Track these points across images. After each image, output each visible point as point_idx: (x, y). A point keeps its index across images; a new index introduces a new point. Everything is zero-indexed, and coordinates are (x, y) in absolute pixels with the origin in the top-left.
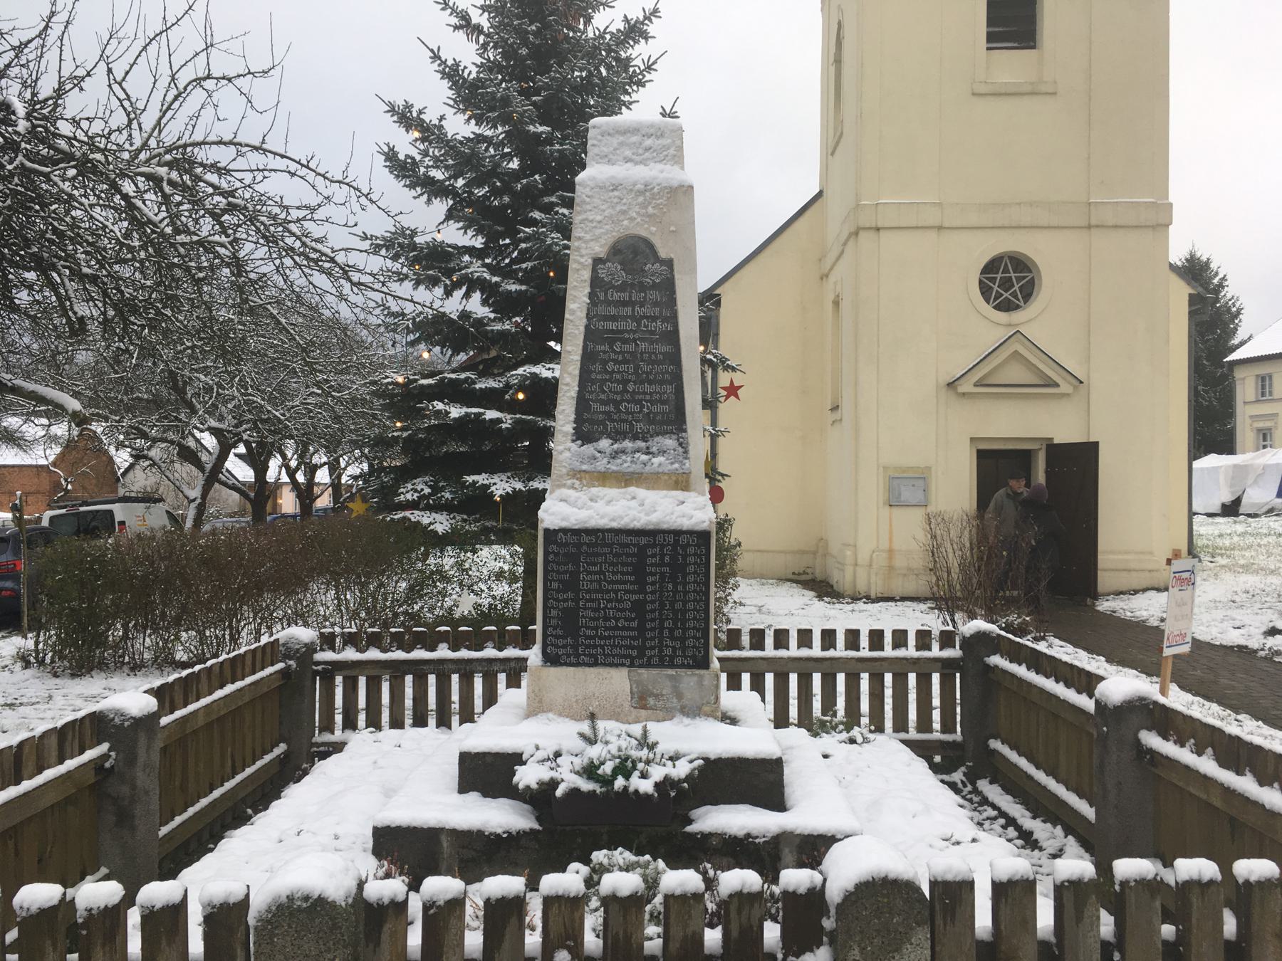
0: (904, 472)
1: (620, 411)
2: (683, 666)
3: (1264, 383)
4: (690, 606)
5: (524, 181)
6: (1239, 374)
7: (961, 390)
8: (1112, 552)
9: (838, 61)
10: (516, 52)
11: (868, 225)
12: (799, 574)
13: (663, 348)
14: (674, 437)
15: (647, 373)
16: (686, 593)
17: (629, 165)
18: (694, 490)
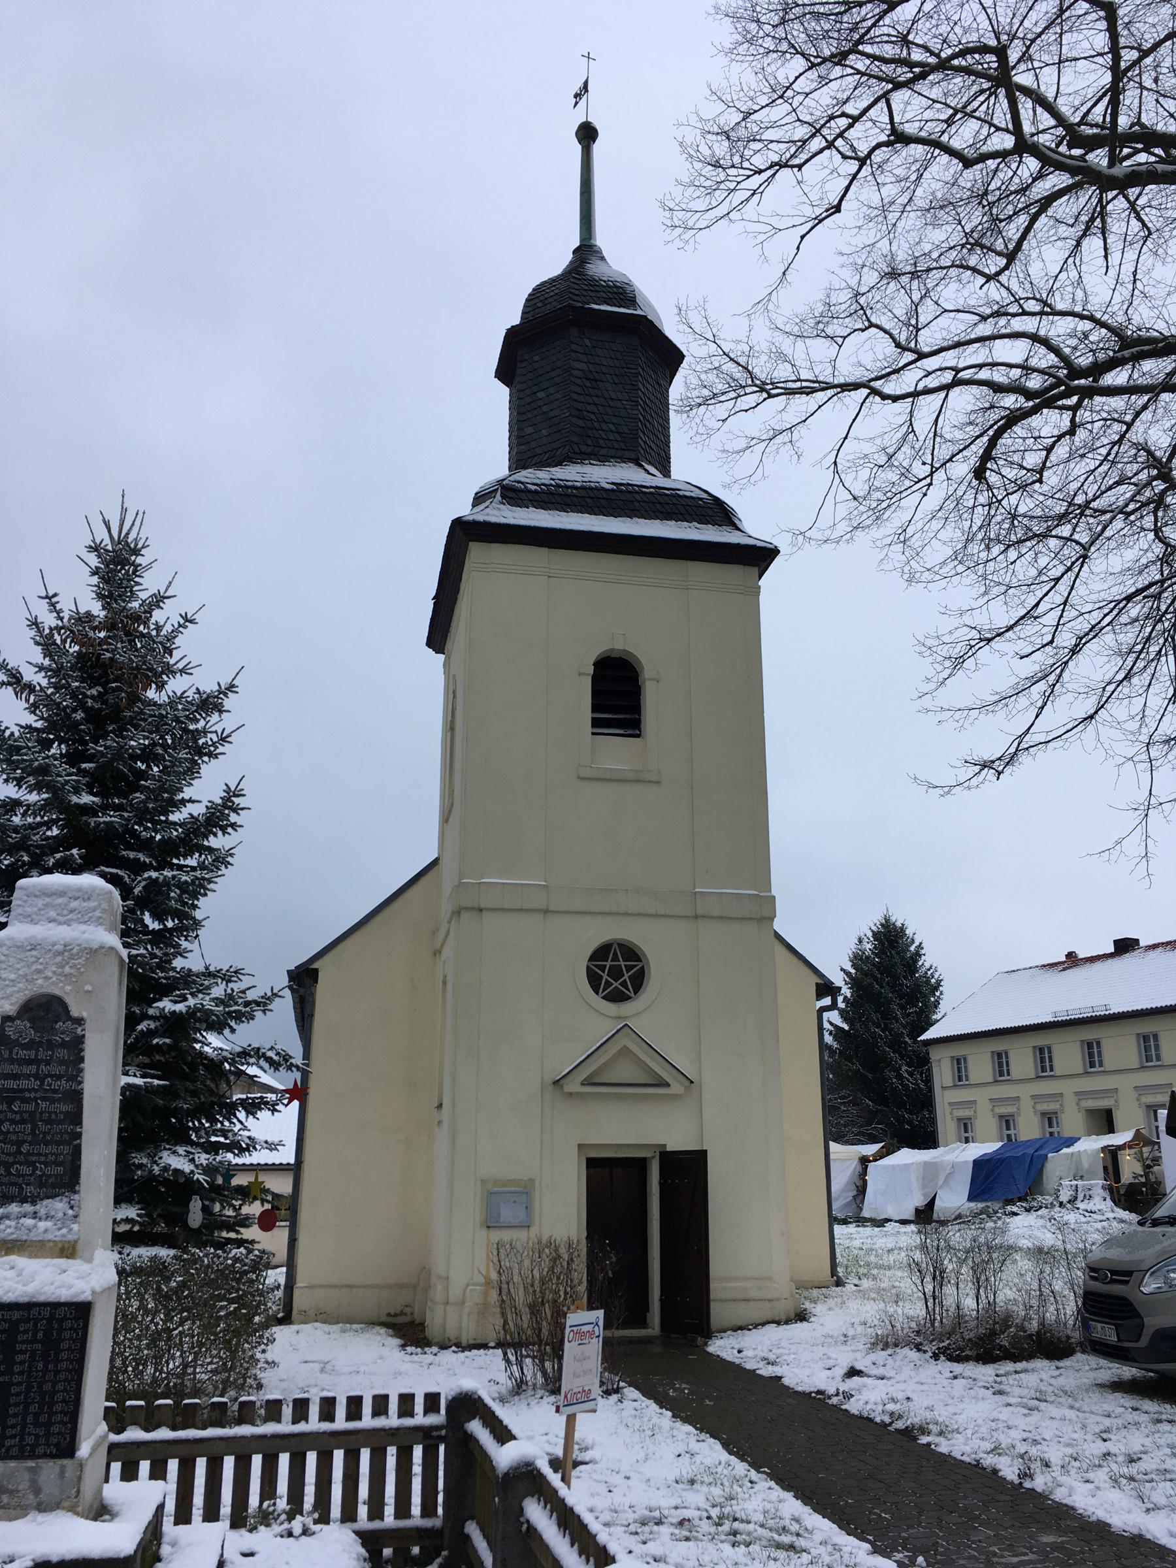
0: (504, 1186)
1: (10, 1174)
2: (44, 1456)
3: (959, 1064)
4: (60, 1387)
5: (58, 856)
6: (935, 1054)
7: (567, 1089)
8: (730, 1279)
9: (452, 729)
10: (68, 717)
11: (470, 905)
12: (396, 1315)
13: (64, 1108)
14: (65, 1199)
15: (45, 1133)
16: (57, 1372)
17: (51, 925)
18: (81, 1258)
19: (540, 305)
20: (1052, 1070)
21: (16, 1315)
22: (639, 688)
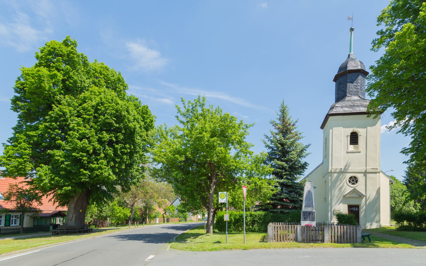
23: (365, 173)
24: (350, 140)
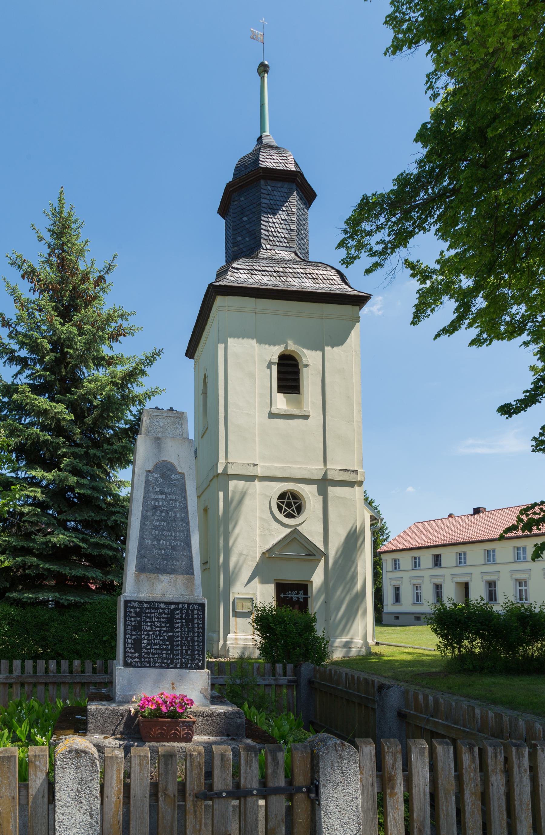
4: (195, 639)
16: (193, 633)
19: (243, 169)
20: (493, 561)
21: (173, 607)
22: (299, 369)
23: (323, 484)
24: (279, 379)
